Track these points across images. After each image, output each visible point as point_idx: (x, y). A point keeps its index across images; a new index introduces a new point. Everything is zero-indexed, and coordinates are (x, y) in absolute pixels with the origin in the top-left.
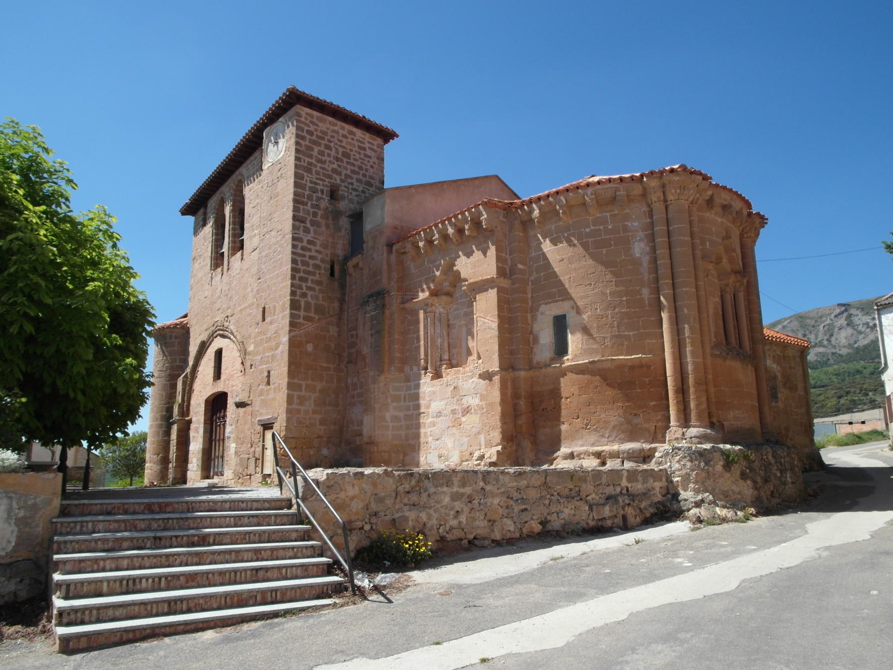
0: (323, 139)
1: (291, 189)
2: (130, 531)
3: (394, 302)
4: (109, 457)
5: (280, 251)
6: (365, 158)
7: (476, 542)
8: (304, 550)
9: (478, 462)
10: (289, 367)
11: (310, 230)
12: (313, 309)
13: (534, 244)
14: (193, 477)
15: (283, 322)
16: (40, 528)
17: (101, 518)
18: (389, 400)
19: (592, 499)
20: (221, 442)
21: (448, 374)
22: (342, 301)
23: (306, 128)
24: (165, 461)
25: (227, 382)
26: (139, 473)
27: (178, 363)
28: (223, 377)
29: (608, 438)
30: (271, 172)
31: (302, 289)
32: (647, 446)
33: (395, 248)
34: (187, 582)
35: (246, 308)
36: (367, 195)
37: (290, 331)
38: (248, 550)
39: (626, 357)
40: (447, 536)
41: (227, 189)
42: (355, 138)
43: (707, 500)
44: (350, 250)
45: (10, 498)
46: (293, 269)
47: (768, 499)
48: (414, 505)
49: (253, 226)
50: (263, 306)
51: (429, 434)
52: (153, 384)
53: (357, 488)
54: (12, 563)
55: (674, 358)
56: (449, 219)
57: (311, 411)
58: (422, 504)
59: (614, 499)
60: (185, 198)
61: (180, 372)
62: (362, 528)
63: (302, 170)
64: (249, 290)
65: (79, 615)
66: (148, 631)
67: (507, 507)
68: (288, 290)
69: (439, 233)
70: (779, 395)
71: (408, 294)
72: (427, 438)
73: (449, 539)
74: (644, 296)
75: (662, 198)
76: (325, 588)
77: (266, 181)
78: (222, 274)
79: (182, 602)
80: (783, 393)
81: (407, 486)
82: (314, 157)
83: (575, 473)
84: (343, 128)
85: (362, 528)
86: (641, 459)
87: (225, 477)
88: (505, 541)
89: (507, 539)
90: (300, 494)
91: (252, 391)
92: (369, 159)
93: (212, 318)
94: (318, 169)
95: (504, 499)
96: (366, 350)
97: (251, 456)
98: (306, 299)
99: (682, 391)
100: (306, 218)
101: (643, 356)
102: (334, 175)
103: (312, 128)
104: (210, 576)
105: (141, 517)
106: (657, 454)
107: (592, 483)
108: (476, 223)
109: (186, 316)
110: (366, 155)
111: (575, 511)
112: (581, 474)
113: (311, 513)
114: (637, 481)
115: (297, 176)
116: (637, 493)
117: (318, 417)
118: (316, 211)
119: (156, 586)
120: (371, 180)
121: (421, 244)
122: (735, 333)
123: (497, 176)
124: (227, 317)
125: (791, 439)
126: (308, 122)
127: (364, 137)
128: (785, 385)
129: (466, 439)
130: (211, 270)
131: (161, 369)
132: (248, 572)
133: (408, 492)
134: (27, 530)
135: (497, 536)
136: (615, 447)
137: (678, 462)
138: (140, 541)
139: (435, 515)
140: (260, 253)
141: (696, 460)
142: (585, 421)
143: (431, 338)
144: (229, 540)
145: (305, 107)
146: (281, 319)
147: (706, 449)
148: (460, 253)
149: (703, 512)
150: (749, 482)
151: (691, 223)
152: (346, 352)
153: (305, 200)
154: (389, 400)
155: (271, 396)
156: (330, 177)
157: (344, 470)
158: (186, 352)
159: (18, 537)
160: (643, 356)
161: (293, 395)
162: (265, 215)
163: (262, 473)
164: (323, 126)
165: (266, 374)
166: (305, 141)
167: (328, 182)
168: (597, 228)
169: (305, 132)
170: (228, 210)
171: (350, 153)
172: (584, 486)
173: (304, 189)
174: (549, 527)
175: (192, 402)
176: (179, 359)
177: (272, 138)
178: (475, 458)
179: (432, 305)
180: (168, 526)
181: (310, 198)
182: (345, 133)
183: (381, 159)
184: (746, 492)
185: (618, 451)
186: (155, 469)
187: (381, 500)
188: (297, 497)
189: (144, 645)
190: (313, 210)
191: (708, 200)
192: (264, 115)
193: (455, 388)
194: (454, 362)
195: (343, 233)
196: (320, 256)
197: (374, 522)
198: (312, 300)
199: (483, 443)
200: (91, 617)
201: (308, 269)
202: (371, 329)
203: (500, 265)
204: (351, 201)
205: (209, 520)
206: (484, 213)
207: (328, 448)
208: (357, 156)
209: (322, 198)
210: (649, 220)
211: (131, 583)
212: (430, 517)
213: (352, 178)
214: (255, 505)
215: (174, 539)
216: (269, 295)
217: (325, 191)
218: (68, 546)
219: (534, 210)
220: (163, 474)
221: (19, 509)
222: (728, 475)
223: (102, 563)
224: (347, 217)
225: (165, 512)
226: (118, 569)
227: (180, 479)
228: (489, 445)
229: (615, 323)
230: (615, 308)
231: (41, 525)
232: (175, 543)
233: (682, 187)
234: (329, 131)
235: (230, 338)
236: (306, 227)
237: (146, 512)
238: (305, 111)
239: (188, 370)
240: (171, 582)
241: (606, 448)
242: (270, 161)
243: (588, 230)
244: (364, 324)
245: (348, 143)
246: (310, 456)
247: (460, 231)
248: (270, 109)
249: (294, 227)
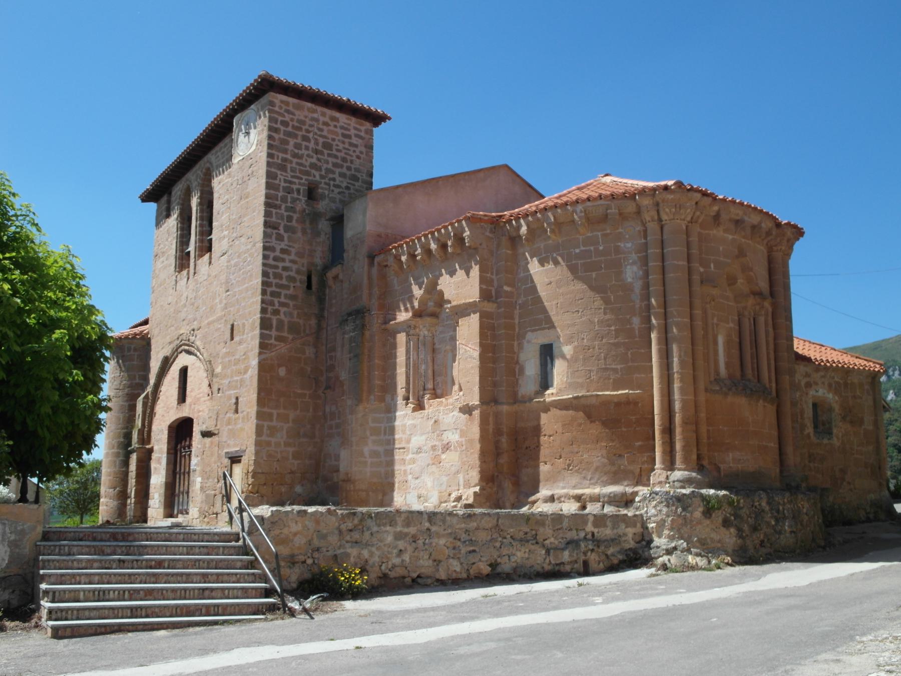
0: (300, 129)
1: (262, 191)
2: (99, 555)
3: (375, 321)
4: (56, 490)
5: (250, 261)
6: (350, 148)
7: (419, 580)
8: (246, 577)
9: (455, 503)
10: (259, 394)
11: (283, 237)
12: (286, 328)
13: (522, 263)
14: (155, 515)
15: (253, 343)
16: (27, 549)
17: (75, 543)
18: (368, 433)
19: (551, 543)
20: (186, 476)
21: (431, 406)
22: (320, 317)
23: (280, 118)
24: (123, 496)
25: (193, 406)
26: (90, 510)
27: (137, 381)
28: (189, 400)
29: (590, 480)
30: (240, 168)
31: (274, 305)
32: (629, 490)
33: (377, 260)
34: (146, 596)
35: (213, 322)
36: (352, 191)
37: (260, 353)
38: (196, 574)
39: (612, 393)
40: (389, 573)
41: (193, 177)
42: (338, 125)
43: (680, 548)
44: (330, 258)
45: (4, 524)
46: (264, 283)
47: (755, 548)
48: (356, 543)
49: (222, 226)
50: (231, 323)
51: (409, 471)
53: (300, 525)
54: (6, 577)
55: (662, 395)
56: (432, 233)
57: (282, 443)
58: (364, 542)
59: (574, 544)
60: (146, 184)
61: (140, 391)
62: (304, 562)
63: (275, 168)
64: (217, 301)
65: (64, 613)
66: (115, 628)
67: (454, 548)
69: (422, 247)
70: (835, 431)
71: (389, 312)
72: (407, 476)
73: (391, 577)
74: (634, 326)
75: (656, 217)
76: (261, 607)
77: (236, 178)
78: (188, 278)
79: (141, 610)
80: (840, 429)
81: (350, 525)
82: (289, 152)
83: (531, 516)
84: (323, 114)
85: (304, 562)
86: (623, 503)
87: (190, 516)
88: (450, 581)
89: (453, 579)
90: (246, 529)
91: (219, 419)
92: (355, 149)
93: (176, 329)
94: (294, 165)
95: (451, 540)
96: (344, 376)
98: (278, 317)
99: (669, 431)
100: (280, 224)
101: (631, 392)
102: (313, 171)
103: (287, 118)
104: (164, 592)
105: (108, 543)
106: (637, 499)
107: (551, 527)
108: (459, 239)
109: (146, 322)
110: (351, 144)
111: (529, 554)
112: (539, 518)
113: (255, 547)
114: (605, 526)
115: (270, 175)
116: (605, 538)
117: (291, 450)
118: (291, 214)
119: (121, 597)
120: (357, 174)
121: (404, 258)
122: (752, 363)
123: (506, 166)
125: (849, 483)
126: (282, 111)
127: (349, 122)
128: (844, 418)
129: (445, 479)
130: (175, 271)
131: (118, 387)
132: (196, 591)
133: (351, 530)
134: (17, 550)
135: (442, 575)
136: (597, 490)
137: (655, 507)
138: (108, 562)
139: (377, 553)
140: (228, 262)
141: (673, 505)
142: (568, 461)
143: (414, 365)
144: (181, 566)
145: (280, 93)
146: (250, 339)
147: (684, 495)
148: (443, 271)
149: (674, 560)
150: (732, 530)
151: (688, 245)
153: (279, 202)
154: (368, 433)
155: (239, 426)
156: (307, 173)
157: (288, 508)
158: (146, 368)
159: (10, 556)
160: (631, 392)
161: (263, 426)
164: (300, 115)
165: (234, 401)
166: (279, 134)
167: (306, 180)
168: (588, 248)
169: (279, 122)
170: (194, 202)
171: (332, 142)
172: (541, 530)
173: (277, 189)
174: (499, 570)
175: (154, 428)
177: (243, 127)
178: (452, 499)
179: (415, 327)
180: (130, 552)
181: (284, 199)
182: (327, 119)
183: (370, 147)
184: (727, 540)
185: (599, 495)
186: (112, 505)
187: (324, 537)
188: (243, 530)
189: (113, 636)
190: (288, 213)
191: (715, 216)
192: (234, 101)
193: (435, 422)
194: (439, 391)
195: (322, 238)
196: (294, 267)
197: (316, 556)
198: (286, 317)
199: (462, 483)
200: (72, 615)
201: (281, 282)
202: (350, 353)
203: (484, 287)
204: (333, 200)
205: (164, 548)
206: (467, 229)
207: (302, 485)
208: (341, 146)
209: (298, 199)
210: (643, 241)
211: (101, 593)
212: (372, 554)
213: (334, 173)
214: (206, 537)
215: (135, 562)
216: (238, 311)
217: (301, 191)
218: (51, 564)
219: (522, 226)
220: (121, 510)
221: (11, 533)
222: (708, 522)
223: (78, 578)
224: (327, 220)
225: (127, 541)
226: (90, 583)
228: (467, 485)
229: (602, 355)
230: (602, 338)
231: (28, 547)
232: (136, 566)
233: (678, 206)
234: (307, 120)
235: (196, 355)
236: (280, 234)
237: (112, 540)
238: (278, 98)
239: (149, 389)
240: (133, 595)
241: (587, 491)
242: (241, 154)
243: (577, 251)
244: (343, 346)
245: (330, 132)
246: (281, 494)
247: (444, 246)
248: (241, 95)
249: (266, 235)
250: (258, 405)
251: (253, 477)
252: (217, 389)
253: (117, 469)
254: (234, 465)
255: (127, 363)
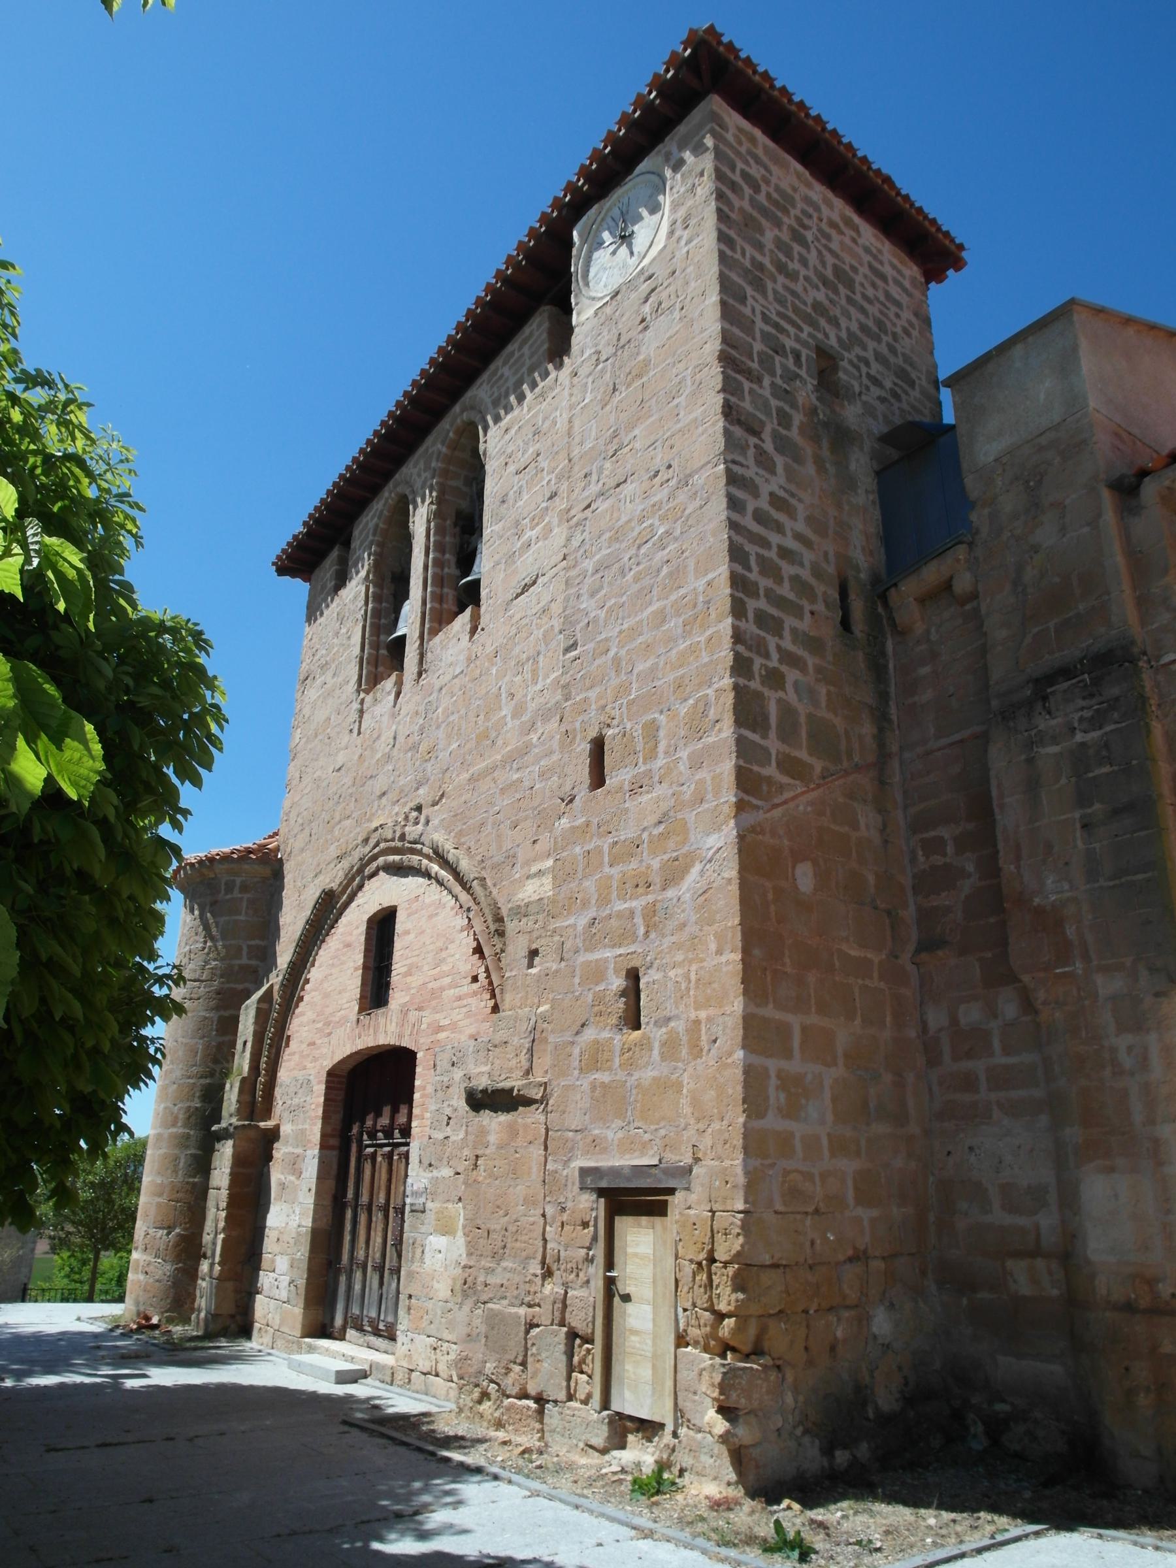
10: (746, 951)
25: (413, 1016)
27: (244, 961)
28: (397, 998)
31: (767, 656)
46: (736, 581)
50: (593, 733)
52: (179, 1009)
68: (725, 654)
93: (358, 823)
97: (543, 1314)
117: (849, 1166)
124: (419, 809)
126: (743, 150)
130: (358, 691)
152: (912, 908)
158: (269, 929)
162: (588, 445)
163: (606, 1404)
165: (617, 983)
170: (420, 521)
175: (283, 1075)
176: (249, 947)
186: (159, 1274)
208: (870, 292)
216: (624, 689)
217: (803, 359)
227: (232, 1316)
239: (275, 979)
246: (833, 1348)
250: (745, 993)
251: (739, 1285)
252: (524, 952)
253: (180, 1177)
254: (623, 1224)
255: (222, 919)
